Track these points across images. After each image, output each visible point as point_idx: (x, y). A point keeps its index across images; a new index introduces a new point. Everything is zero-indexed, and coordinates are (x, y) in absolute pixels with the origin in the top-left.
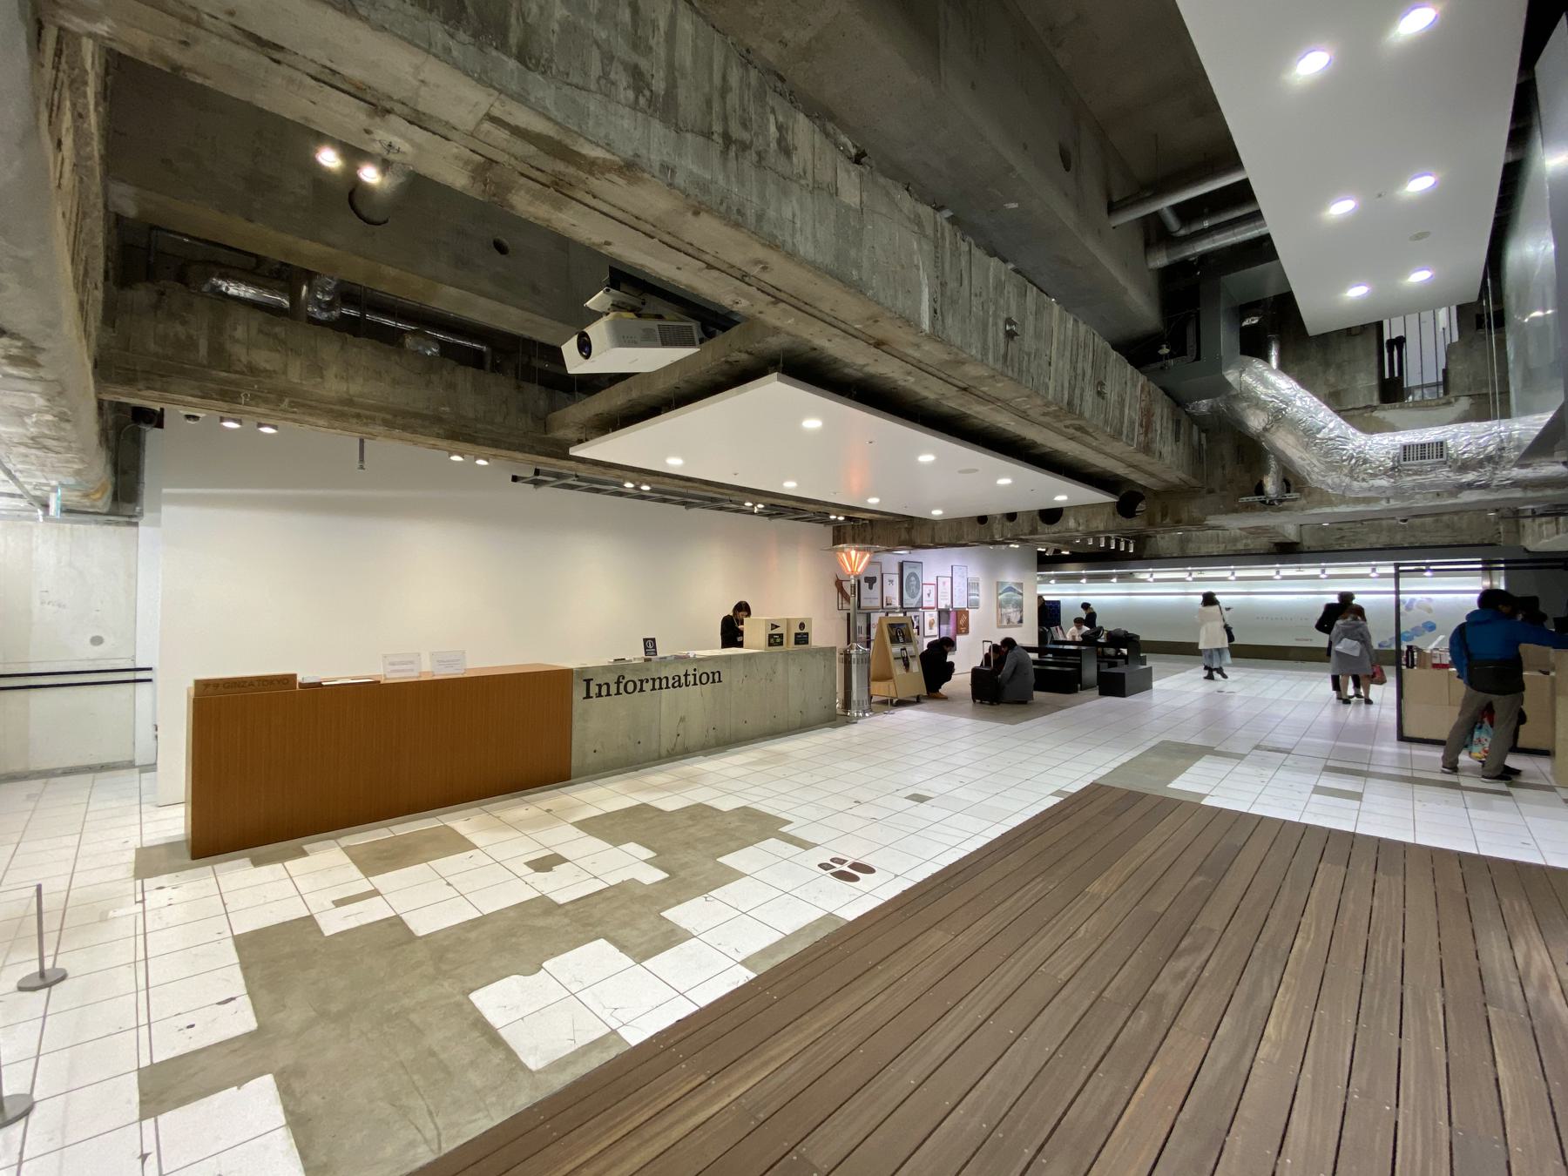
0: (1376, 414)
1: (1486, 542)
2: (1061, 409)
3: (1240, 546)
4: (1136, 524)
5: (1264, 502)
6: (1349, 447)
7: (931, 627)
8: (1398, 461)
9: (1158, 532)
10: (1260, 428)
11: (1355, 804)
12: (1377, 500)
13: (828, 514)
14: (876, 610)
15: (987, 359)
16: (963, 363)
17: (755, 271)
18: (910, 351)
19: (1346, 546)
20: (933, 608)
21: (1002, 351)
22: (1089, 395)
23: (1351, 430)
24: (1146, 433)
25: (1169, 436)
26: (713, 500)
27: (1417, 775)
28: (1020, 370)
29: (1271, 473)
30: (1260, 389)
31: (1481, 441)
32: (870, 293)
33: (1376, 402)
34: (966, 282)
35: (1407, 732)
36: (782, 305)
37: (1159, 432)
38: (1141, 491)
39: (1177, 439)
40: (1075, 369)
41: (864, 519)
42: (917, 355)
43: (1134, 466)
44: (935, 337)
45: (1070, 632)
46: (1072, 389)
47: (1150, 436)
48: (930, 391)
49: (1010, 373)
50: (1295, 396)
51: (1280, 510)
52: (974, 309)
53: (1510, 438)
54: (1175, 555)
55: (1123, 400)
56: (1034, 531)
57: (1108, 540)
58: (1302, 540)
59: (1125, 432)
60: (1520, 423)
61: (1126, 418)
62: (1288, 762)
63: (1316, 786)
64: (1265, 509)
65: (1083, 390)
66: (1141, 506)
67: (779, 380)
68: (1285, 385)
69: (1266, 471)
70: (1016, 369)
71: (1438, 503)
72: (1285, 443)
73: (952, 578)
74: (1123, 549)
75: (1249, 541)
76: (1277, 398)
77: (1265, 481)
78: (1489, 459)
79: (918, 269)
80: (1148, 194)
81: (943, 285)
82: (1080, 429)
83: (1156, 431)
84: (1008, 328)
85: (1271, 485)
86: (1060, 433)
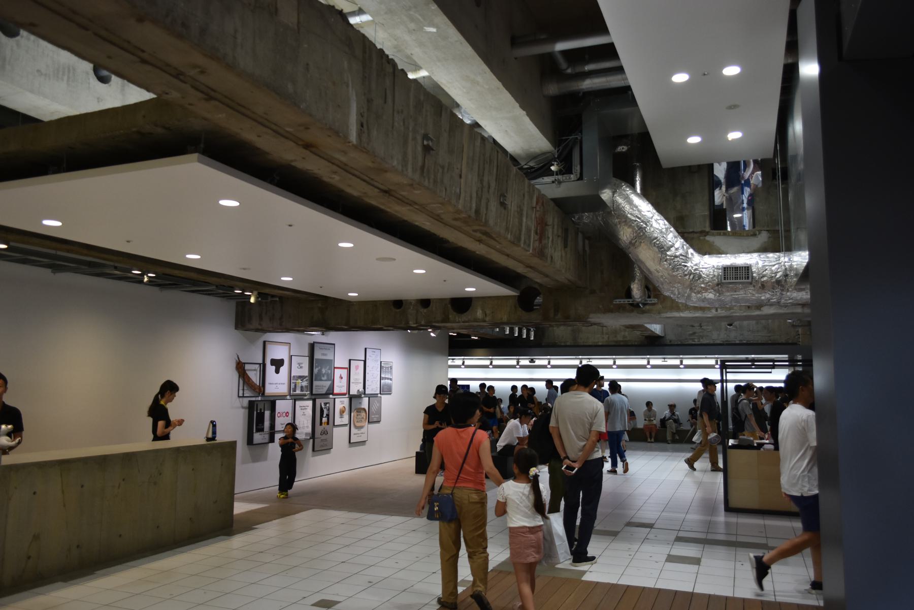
0: (708, 238)
1: (790, 342)
2: (470, 217)
3: (620, 338)
4: (535, 317)
5: (632, 305)
6: (689, 264)
7: (341, 416)
8: (721, 280)
9: (551, 326)
10: (627, 242)
11: (693, 568)
12: (709, 309)
13: (232, 288)
14: (282, 397)
15: (407, 170)
16: (386, 171)
17: (193, 73)
18: (338, 156)
19: (696, 342)
20: (344, 394)
21: (420, 164)
22: (494, 206)
23: (691, 251)
24: (540, 240)
25: (560, 243)
26: (90, 264)
27: (741, 539)
28: (435, 182)
29: (636, 281)
30: (627, 208)
31: (773, 268)
32: (303, 106)
33: (708, 229)
34: (389, 100)
35: (733, 503)
36: (213, 103)
37: (551, 239)
38: (538, 288)
39: (566, 246)
40: (482, 181)
41: (273, 296)
42: (343, 159)
43: (531, 267)
44: (360, 147)
45: (519, 393)
46: (479, 199)
47: (544, 242)
48: (355, 189)
49: (426, 183)
50: (652, 218)
51: (643, 312)
52: (396, 124)
53: (791, 266)
54: (568, 344)
55: (522, 210)
56: (446, 319)
57: (512, 330)
58: (665, 335)
59: (523, 238)
60: (800, 256)
61: (524, 224)
62: (651, 536)
63: (669, 555)
64: (632, 311)
65: (488, 200)
66: (539, 300)
67: (199, 161)
68: (645, 208)
69: (633, 279)
70: (431, 181)
71: (749, 314)
72: (645, 255)
73: (365, 362)
74: (525, 336)
75: (627, 334)
76: (639, 218)
77: (632, 287)
78: (778, 282)
79: (348, 86)
80: (543, 37)
81: (369, 101)
82: (486, 234)
83: (548, 238)
84: (425, 143)
85: (636, 290)
86: (470, 236)
